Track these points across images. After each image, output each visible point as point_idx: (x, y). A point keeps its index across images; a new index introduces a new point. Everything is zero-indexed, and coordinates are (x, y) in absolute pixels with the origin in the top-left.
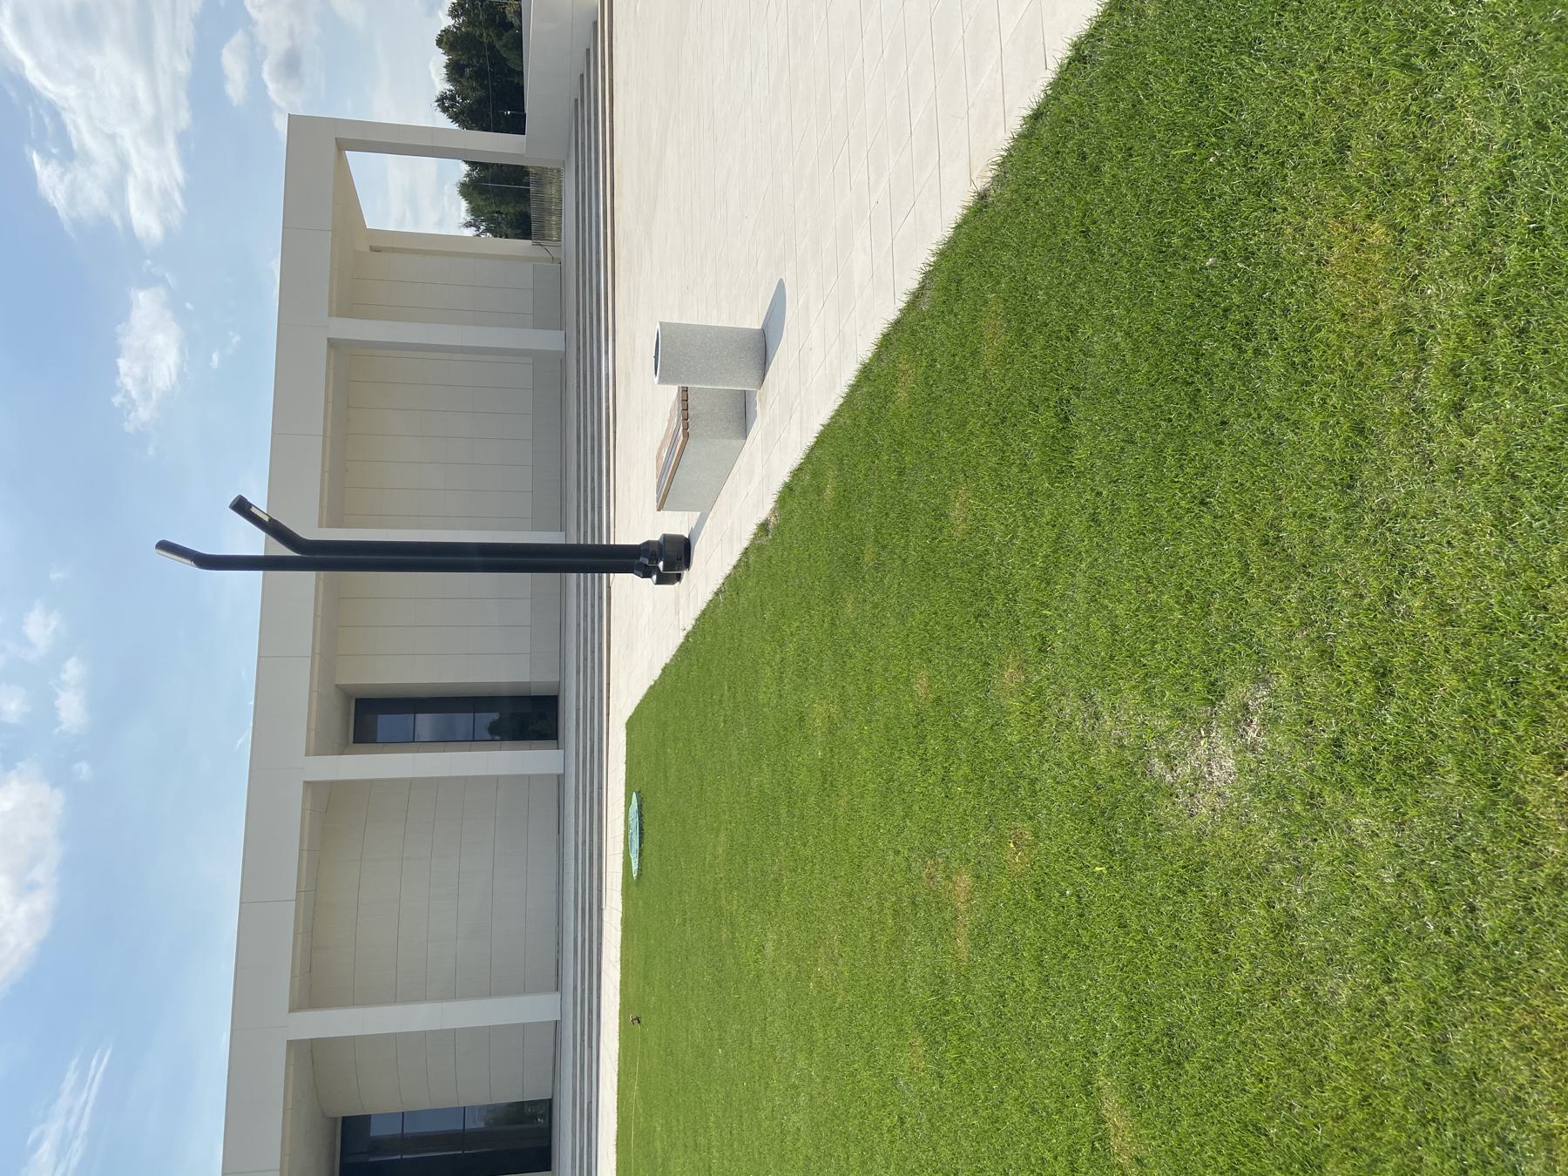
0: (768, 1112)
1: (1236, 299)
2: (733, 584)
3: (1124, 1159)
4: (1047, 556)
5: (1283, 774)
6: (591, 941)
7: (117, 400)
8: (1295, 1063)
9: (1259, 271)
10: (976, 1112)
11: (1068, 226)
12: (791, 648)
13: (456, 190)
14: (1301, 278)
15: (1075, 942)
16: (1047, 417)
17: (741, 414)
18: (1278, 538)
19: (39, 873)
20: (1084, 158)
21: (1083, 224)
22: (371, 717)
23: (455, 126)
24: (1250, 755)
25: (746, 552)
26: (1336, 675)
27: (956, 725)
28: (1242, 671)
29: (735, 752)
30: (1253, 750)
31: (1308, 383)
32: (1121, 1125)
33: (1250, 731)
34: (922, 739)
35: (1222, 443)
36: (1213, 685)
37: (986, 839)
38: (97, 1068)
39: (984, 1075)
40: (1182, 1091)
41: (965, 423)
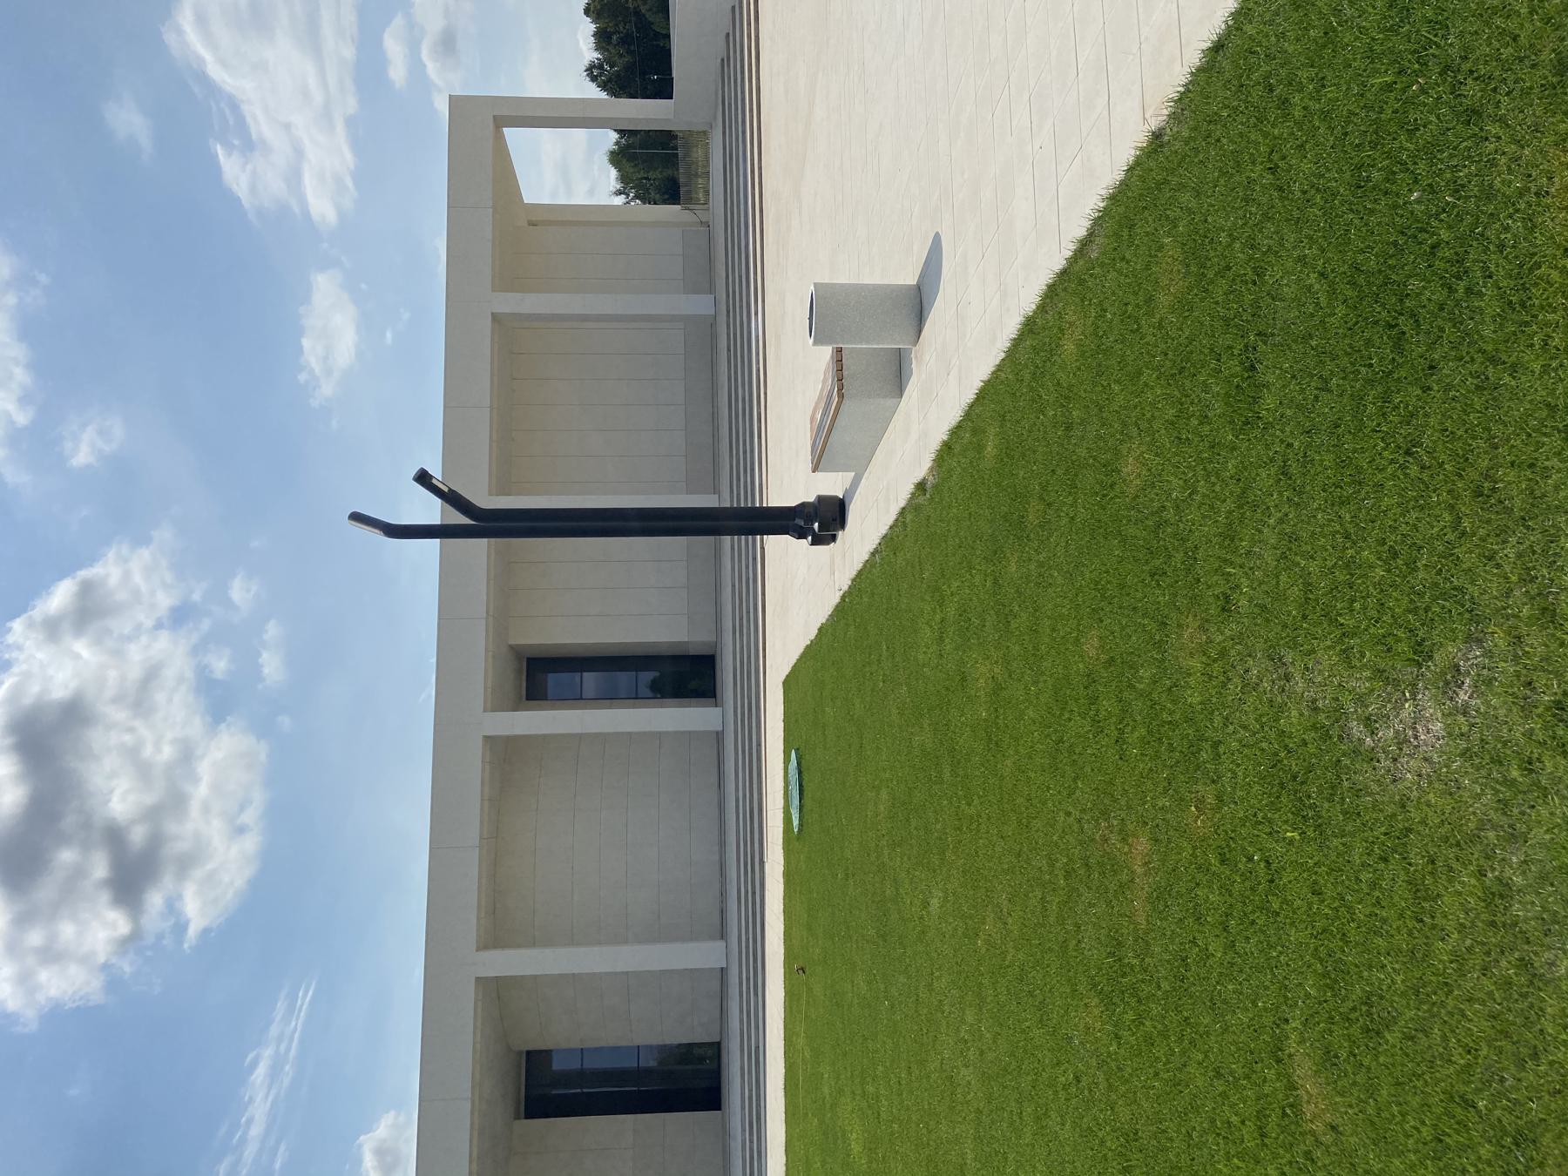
0: (937, 1064)
1: (1444, 235)
2: (890, 542)
3: (1318, 1126)
4: (1230, 512)
5: (1498, 739)
6: (754, 893)
7: (302, 377)
8: (1507, 1035)
9: (1472, 205)
10: (1157, 1074)
11: (1253, 163)
12: (951, 611)
13: (606, 159)
14: (1517, 211)
15: (1264, 908)
16: (1233, 366)
17: (896, 373)
18: (1494, 490)
19: (249, 817)
20: (1271, 91)
21: (1271, 161)
22: (542, 675)
23: (603, 95)
24: (1461, 719)
25: (903, 512)
26: (1559, 634)
27: (1131, 686)
28: (1453, 631)
29: (895, 711)
30: (1465, 714)
31: (1527, 324)
32: (1314, 1092)
33: (1461, 693)
34: (1094, 700)
35: (1429, 388)
36: (1420, 644)
37: (1164, 802)
38: (306, 992)
39: (1167, 1037)
40: (1381, 1060)
41: (1140, 373)
